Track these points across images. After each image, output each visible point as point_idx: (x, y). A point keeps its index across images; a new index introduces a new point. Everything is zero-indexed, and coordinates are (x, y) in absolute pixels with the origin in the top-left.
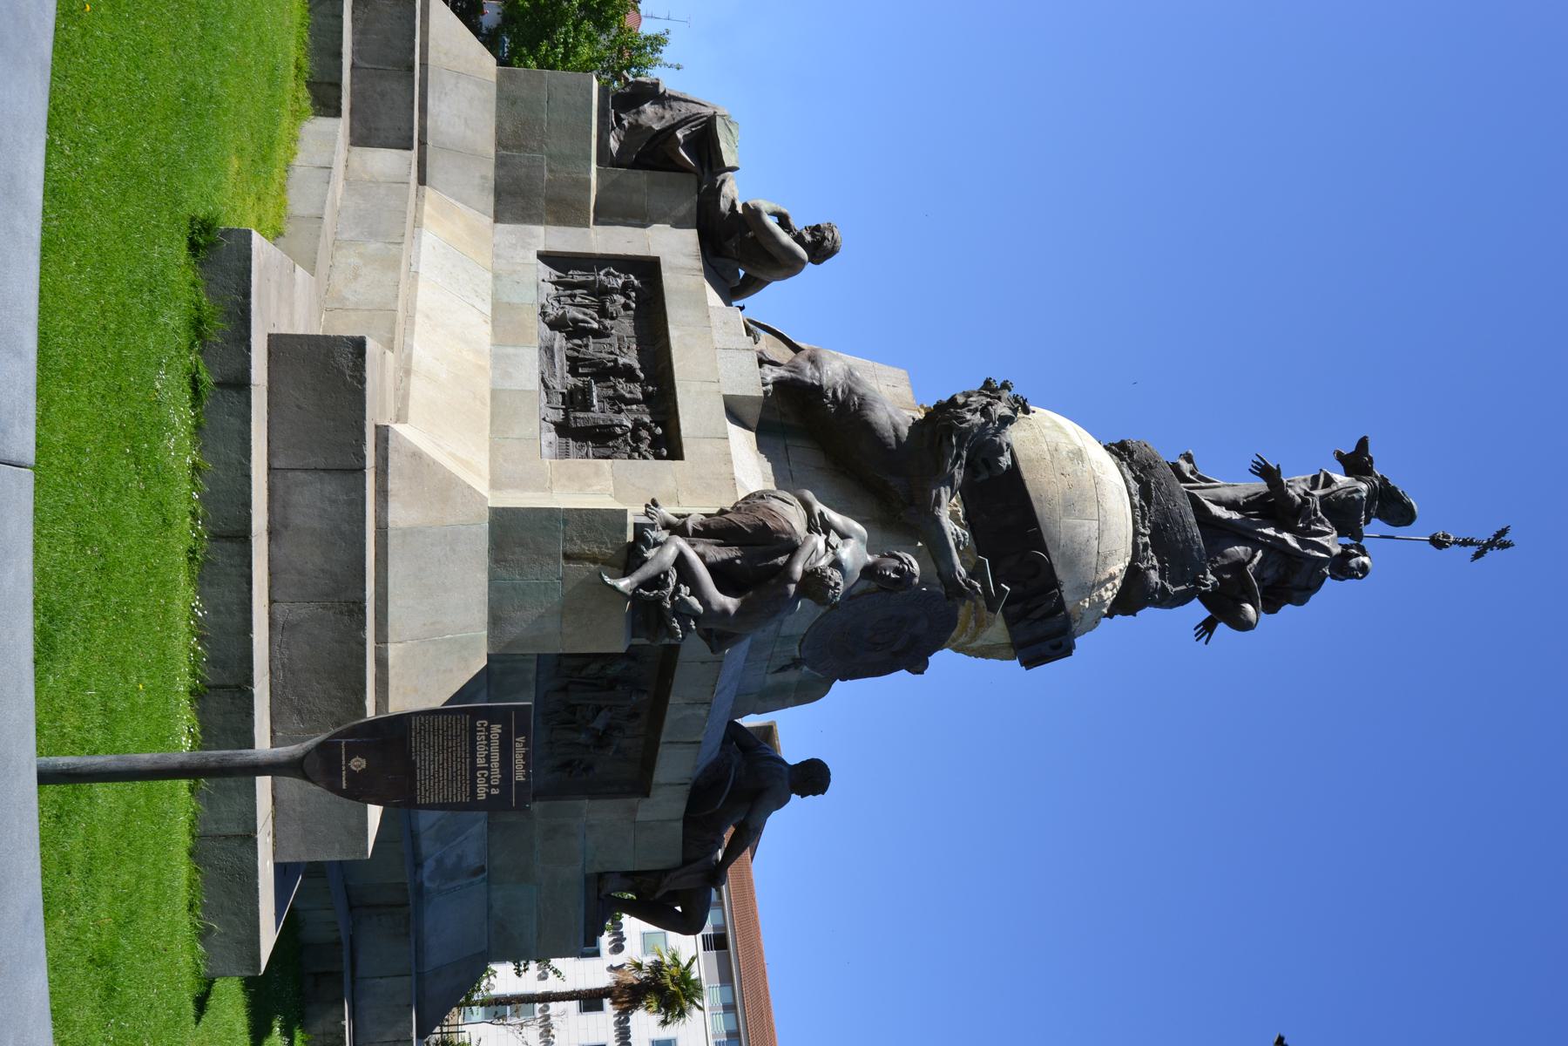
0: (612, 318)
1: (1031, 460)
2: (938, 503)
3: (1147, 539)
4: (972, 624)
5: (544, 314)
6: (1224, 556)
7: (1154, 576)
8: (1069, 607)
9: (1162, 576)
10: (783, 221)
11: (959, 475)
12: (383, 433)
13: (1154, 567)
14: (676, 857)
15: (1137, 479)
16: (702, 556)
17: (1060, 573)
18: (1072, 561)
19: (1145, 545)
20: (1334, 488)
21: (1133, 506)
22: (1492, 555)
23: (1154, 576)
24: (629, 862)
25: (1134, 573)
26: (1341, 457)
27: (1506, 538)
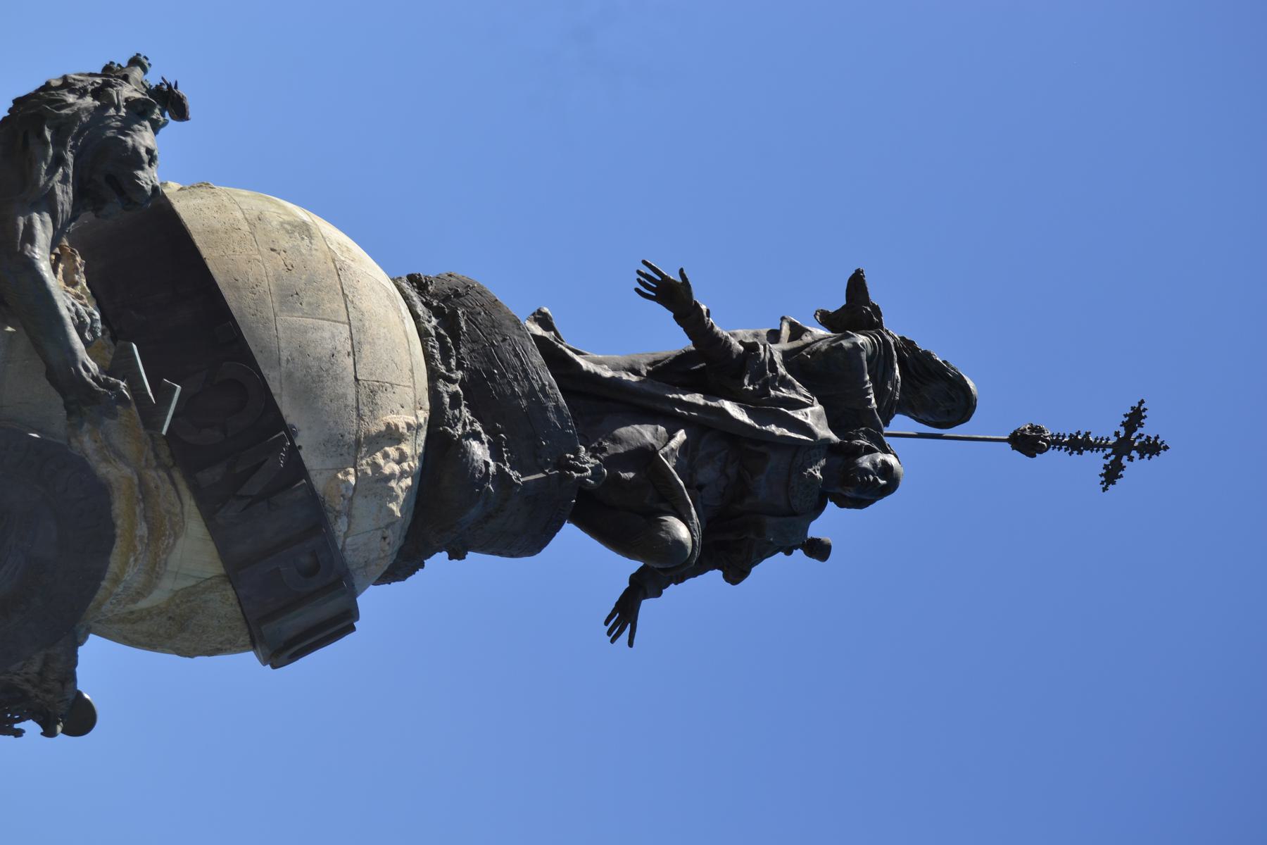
1: (213, 231)
2: (30, 237)
3: (457, 387)
4: (142, 530)
6: (616, 440)
7: (479, 451)
8: (319, 483)
9: (496, 453)
11: (64, 196)
15: (437, 312)
17: (289, 411)
18: (311, 387)
19: (454, 396)
20: (807, 339)
21: (423, 334)
22: (1135, 467)
23: (479, 451)
25: (441, 446)
27: (1148, 429)
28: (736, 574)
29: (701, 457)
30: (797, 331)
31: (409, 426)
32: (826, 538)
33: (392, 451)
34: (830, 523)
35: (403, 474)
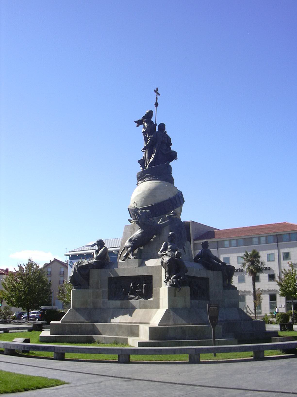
14: (220, 272)
22: (159, 92)
24: (221, 281)
29: (159, 155)
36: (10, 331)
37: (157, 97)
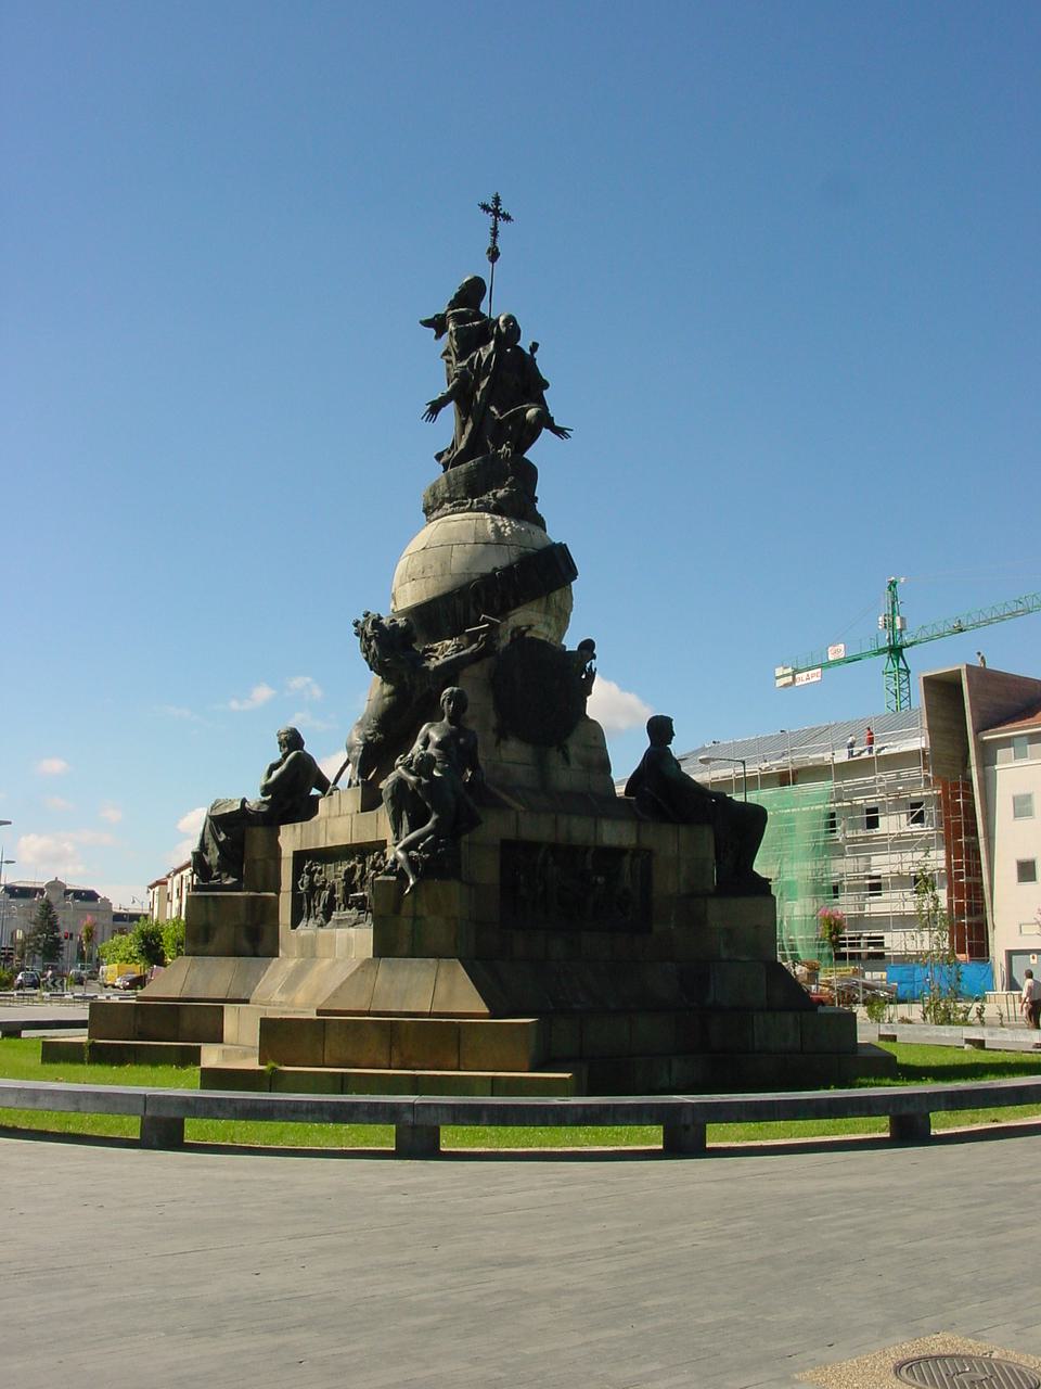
0: (326, 881)
3: (475, 500)
5: (321, 926)
7: (501, 493)
10: (274, 767)
12: (319, 1012)
13: (494, 495)
16: (407, 835)
22: (504, 208)
23: (501, 493)
25: (497, 510)
26: (438, 336)
27: (490, 203)
28: (546, 385)
29: (497, 402)
30: (447, 353)
31: (492, 522)
32: (530, 344)
33: (503, 529)
34: (524, 344)
35: (510, 525)
36: (25, 1034)
37: (496, 228)
